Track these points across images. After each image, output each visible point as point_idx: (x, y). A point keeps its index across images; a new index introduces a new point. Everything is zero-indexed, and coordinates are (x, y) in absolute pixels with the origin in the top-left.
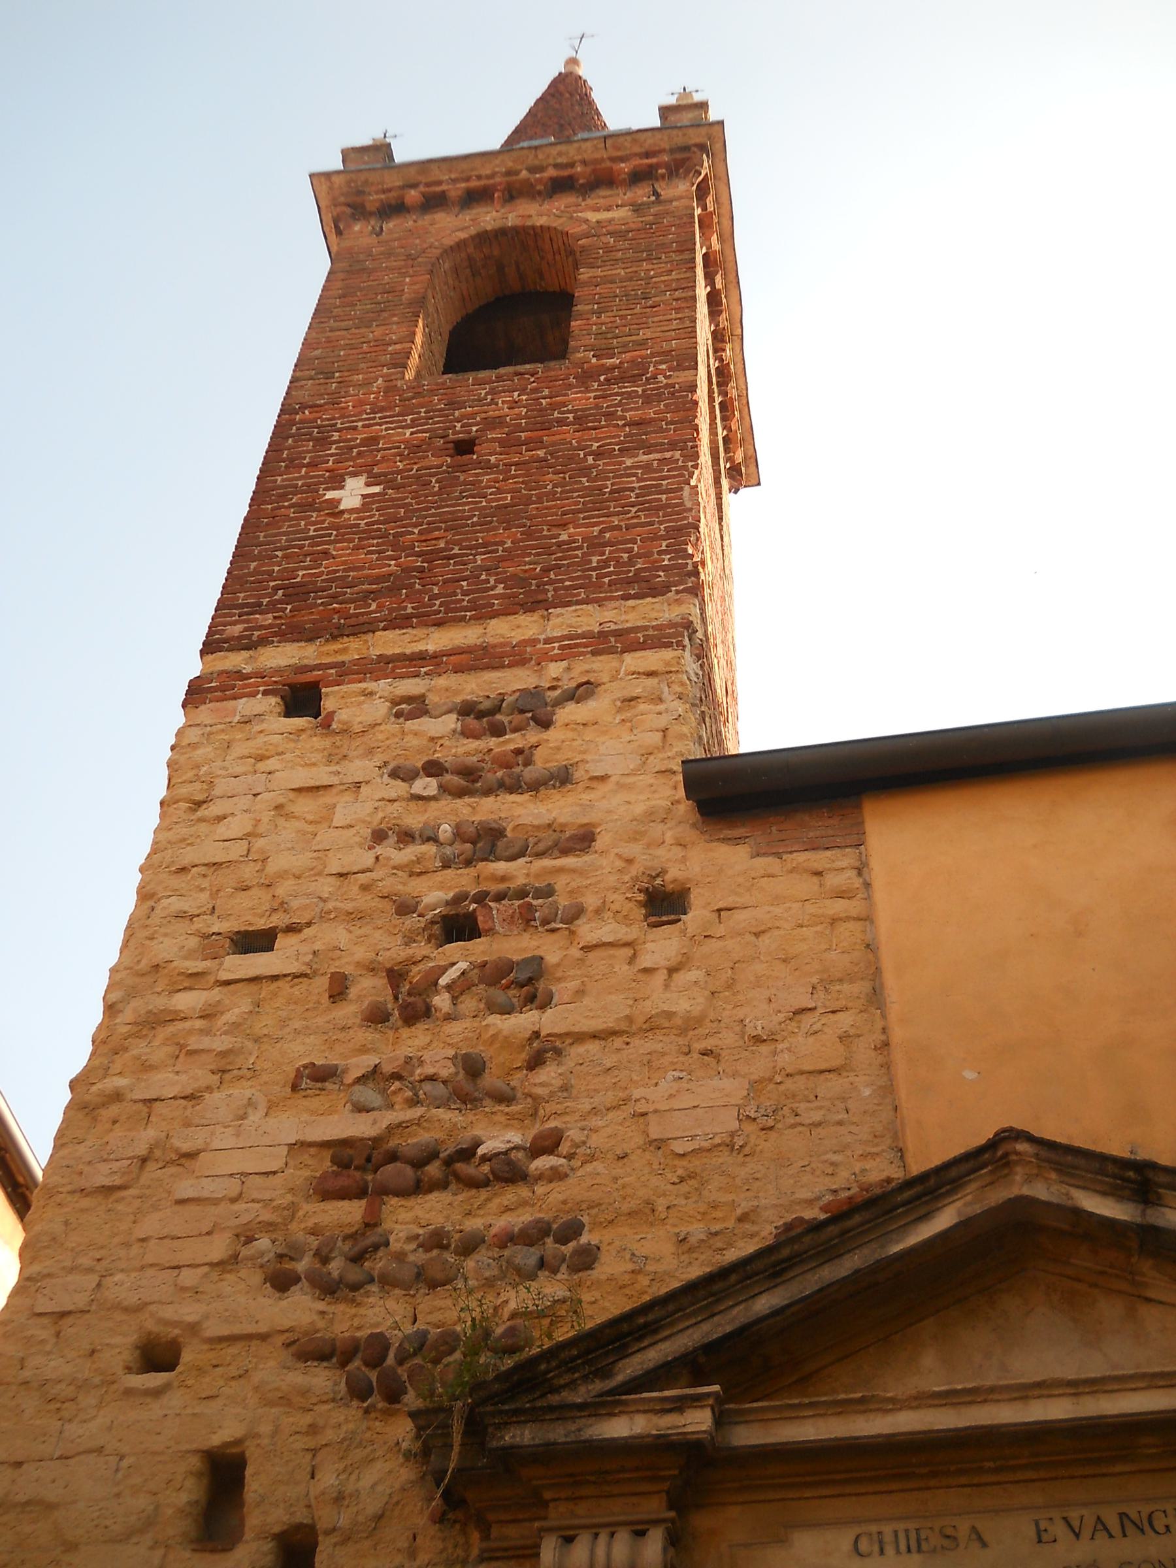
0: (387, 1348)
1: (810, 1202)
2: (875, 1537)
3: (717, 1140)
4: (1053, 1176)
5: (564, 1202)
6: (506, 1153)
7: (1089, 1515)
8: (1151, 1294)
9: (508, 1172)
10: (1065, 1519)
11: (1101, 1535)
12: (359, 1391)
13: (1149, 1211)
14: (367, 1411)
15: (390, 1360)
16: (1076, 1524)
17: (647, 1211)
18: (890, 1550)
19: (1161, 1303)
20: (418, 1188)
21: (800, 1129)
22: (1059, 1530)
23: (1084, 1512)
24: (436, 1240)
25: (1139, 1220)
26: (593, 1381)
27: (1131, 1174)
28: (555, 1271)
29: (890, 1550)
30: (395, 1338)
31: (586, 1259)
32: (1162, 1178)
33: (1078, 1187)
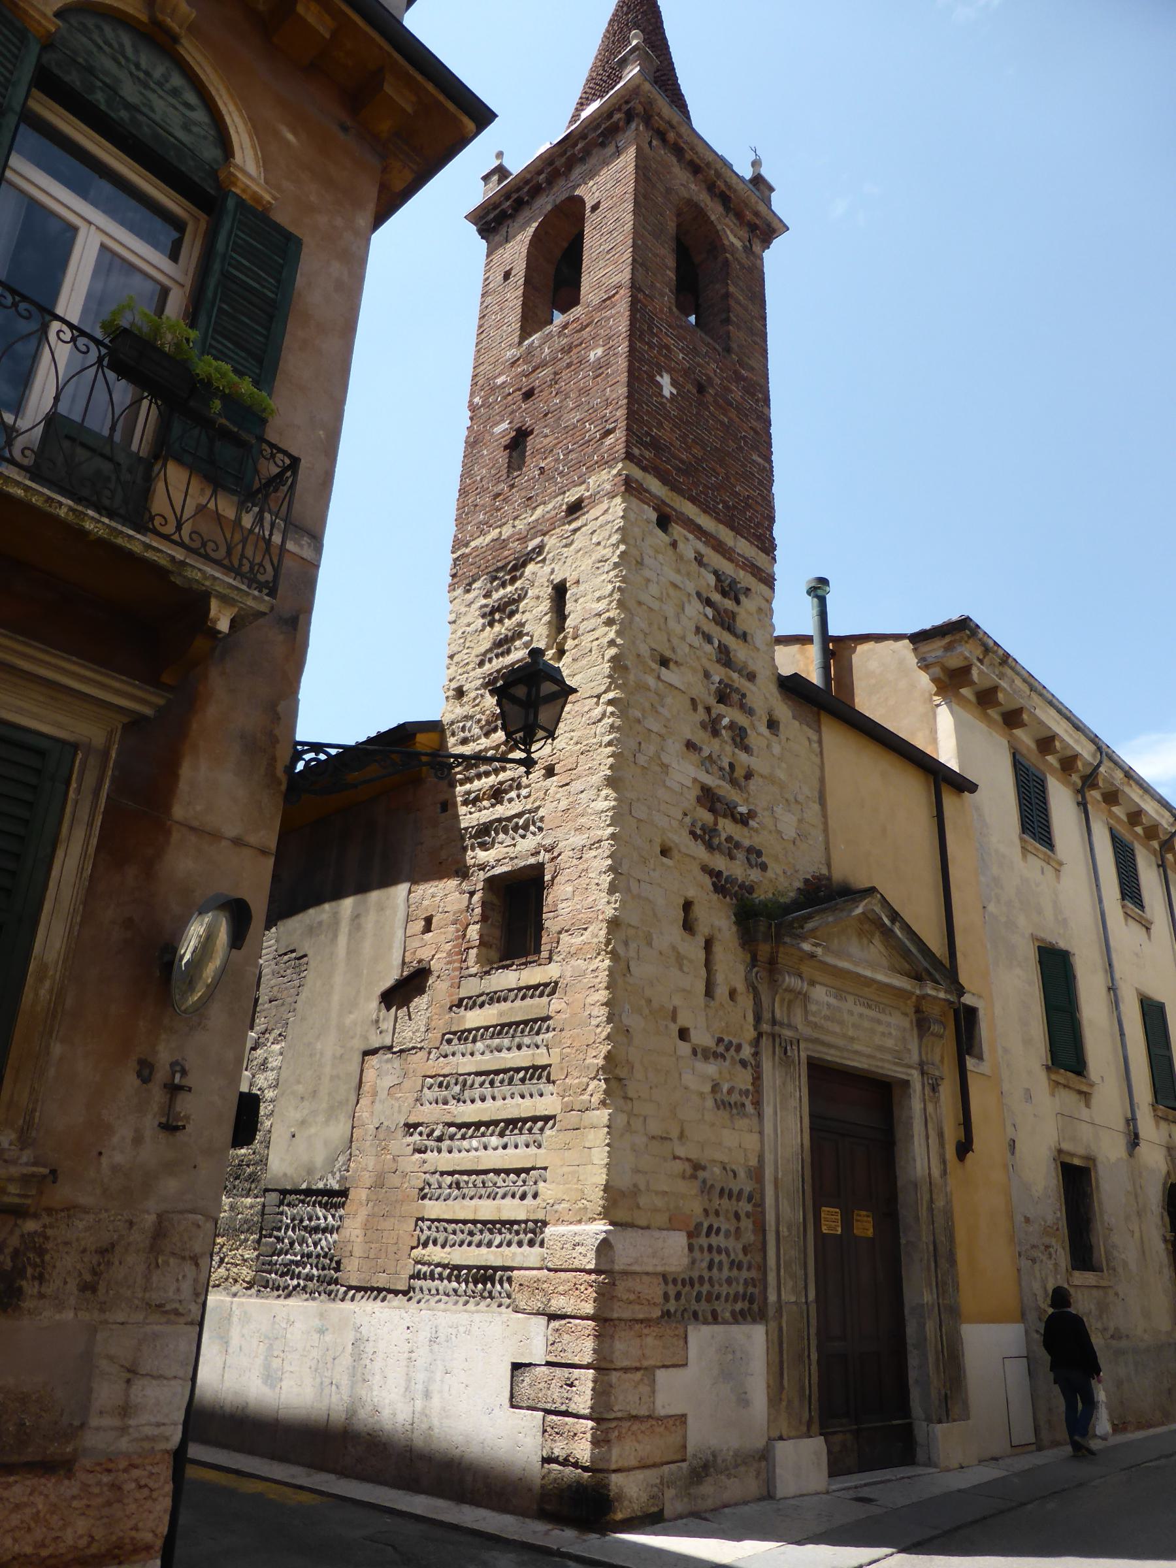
24: (729, 839)
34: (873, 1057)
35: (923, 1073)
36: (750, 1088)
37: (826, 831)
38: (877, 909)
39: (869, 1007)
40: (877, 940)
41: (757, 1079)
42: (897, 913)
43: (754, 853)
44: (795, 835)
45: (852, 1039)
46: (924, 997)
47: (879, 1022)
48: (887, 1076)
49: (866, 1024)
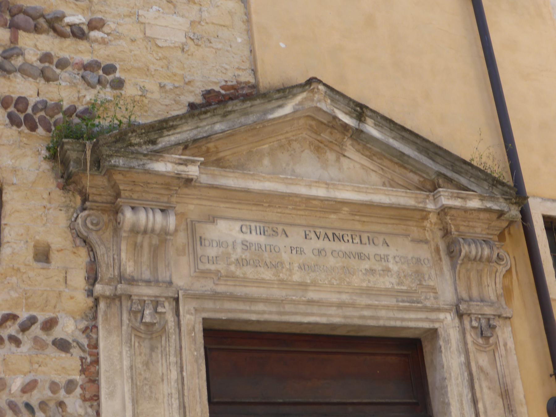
0: (27, 104)
1: (216, 83)
2: (248, 227)
3: (177, 45)
4: (329, 101)
5: (108, 56)
6: (79, 25)
7: (323, 232)
8: (346, 154)
9: (78, 33)
10: (315, 232)
11: (326, 239)
12: (13, 121)
13: (361, 124)
14: (19, 132)
15: (29, 111)
16: (318, 234)
17: (146, 70)
18: (254, 232)
19: (349, 158)
20: (37, 30)
21: (212, 49)
22: (313, 235)
23: (321, 230)
24: (46, 58)
25: (357, 127)
26: (148, 145)
27: (358, 109)
28: (104, 87)
29: (254, 232)
30: (33, 101)
31: (119, 84)
32: (369, 113)
33: (337, 108)
34: (353, 305)
35: (460, 315)
36: (79, 378)
37: (249, 31)
38: (326, 105)
39: (341, 239)
40: (351, 151)
41: (91, 368)
42: (362, 107)
43: (101, 73)
44: (184, 40)
45: (303, 286)
46: (444, 211)
47: (360, 256)
48: (386, 328)
49: (332, 261)
